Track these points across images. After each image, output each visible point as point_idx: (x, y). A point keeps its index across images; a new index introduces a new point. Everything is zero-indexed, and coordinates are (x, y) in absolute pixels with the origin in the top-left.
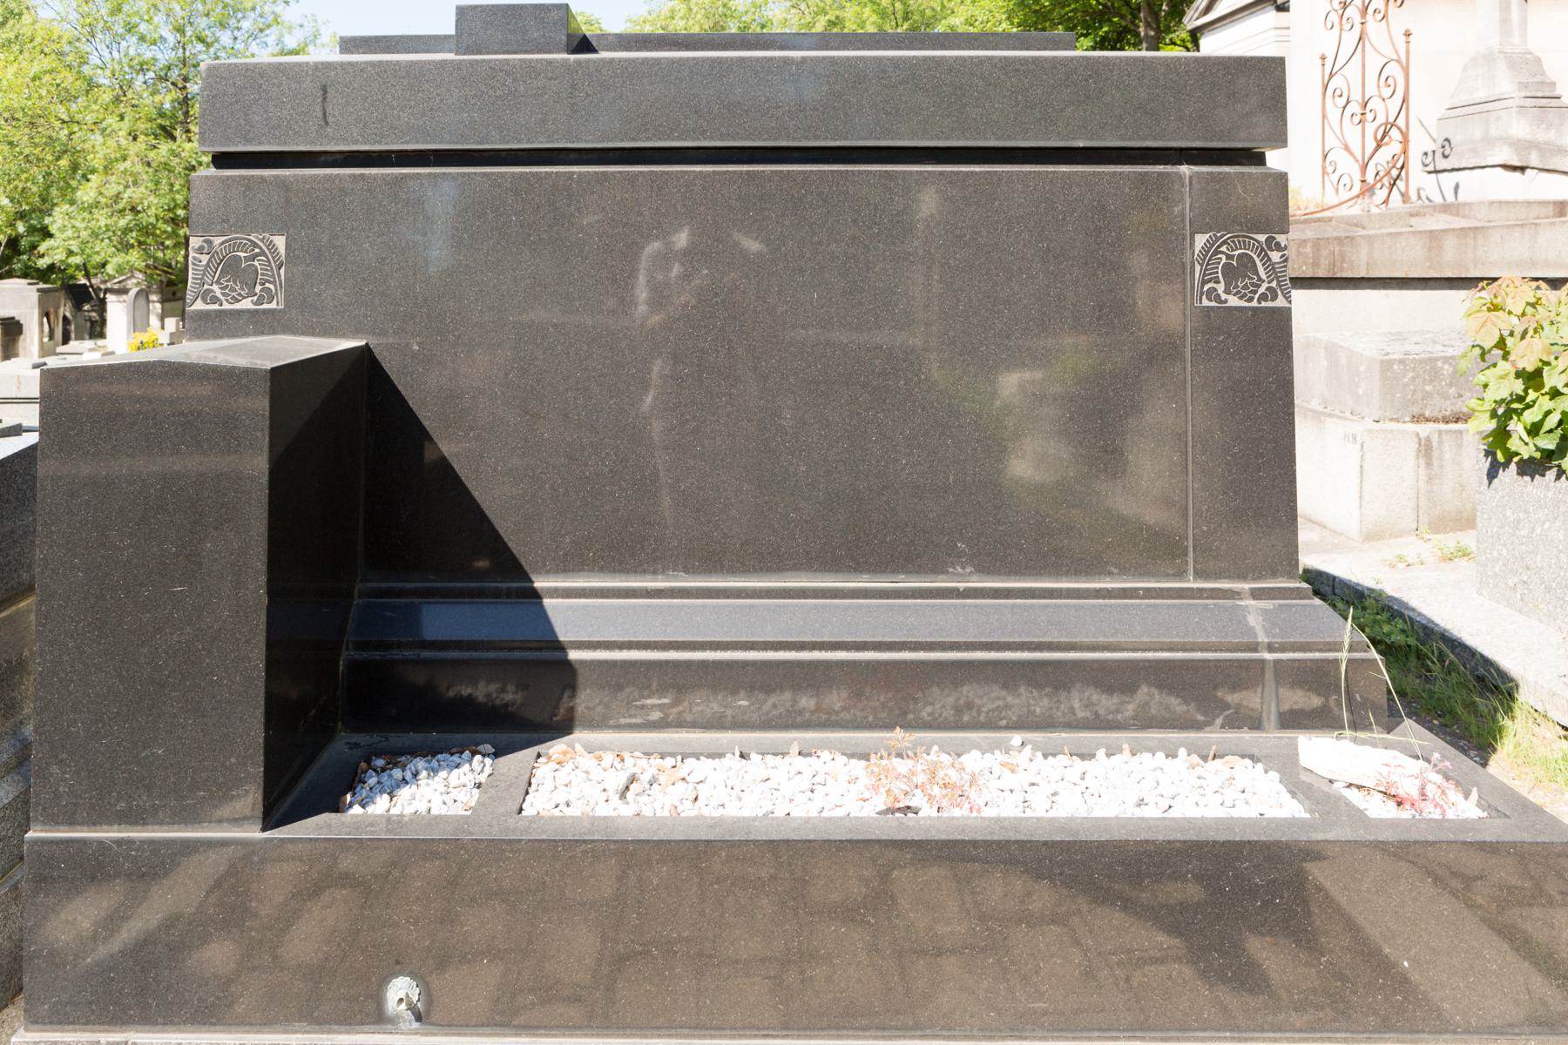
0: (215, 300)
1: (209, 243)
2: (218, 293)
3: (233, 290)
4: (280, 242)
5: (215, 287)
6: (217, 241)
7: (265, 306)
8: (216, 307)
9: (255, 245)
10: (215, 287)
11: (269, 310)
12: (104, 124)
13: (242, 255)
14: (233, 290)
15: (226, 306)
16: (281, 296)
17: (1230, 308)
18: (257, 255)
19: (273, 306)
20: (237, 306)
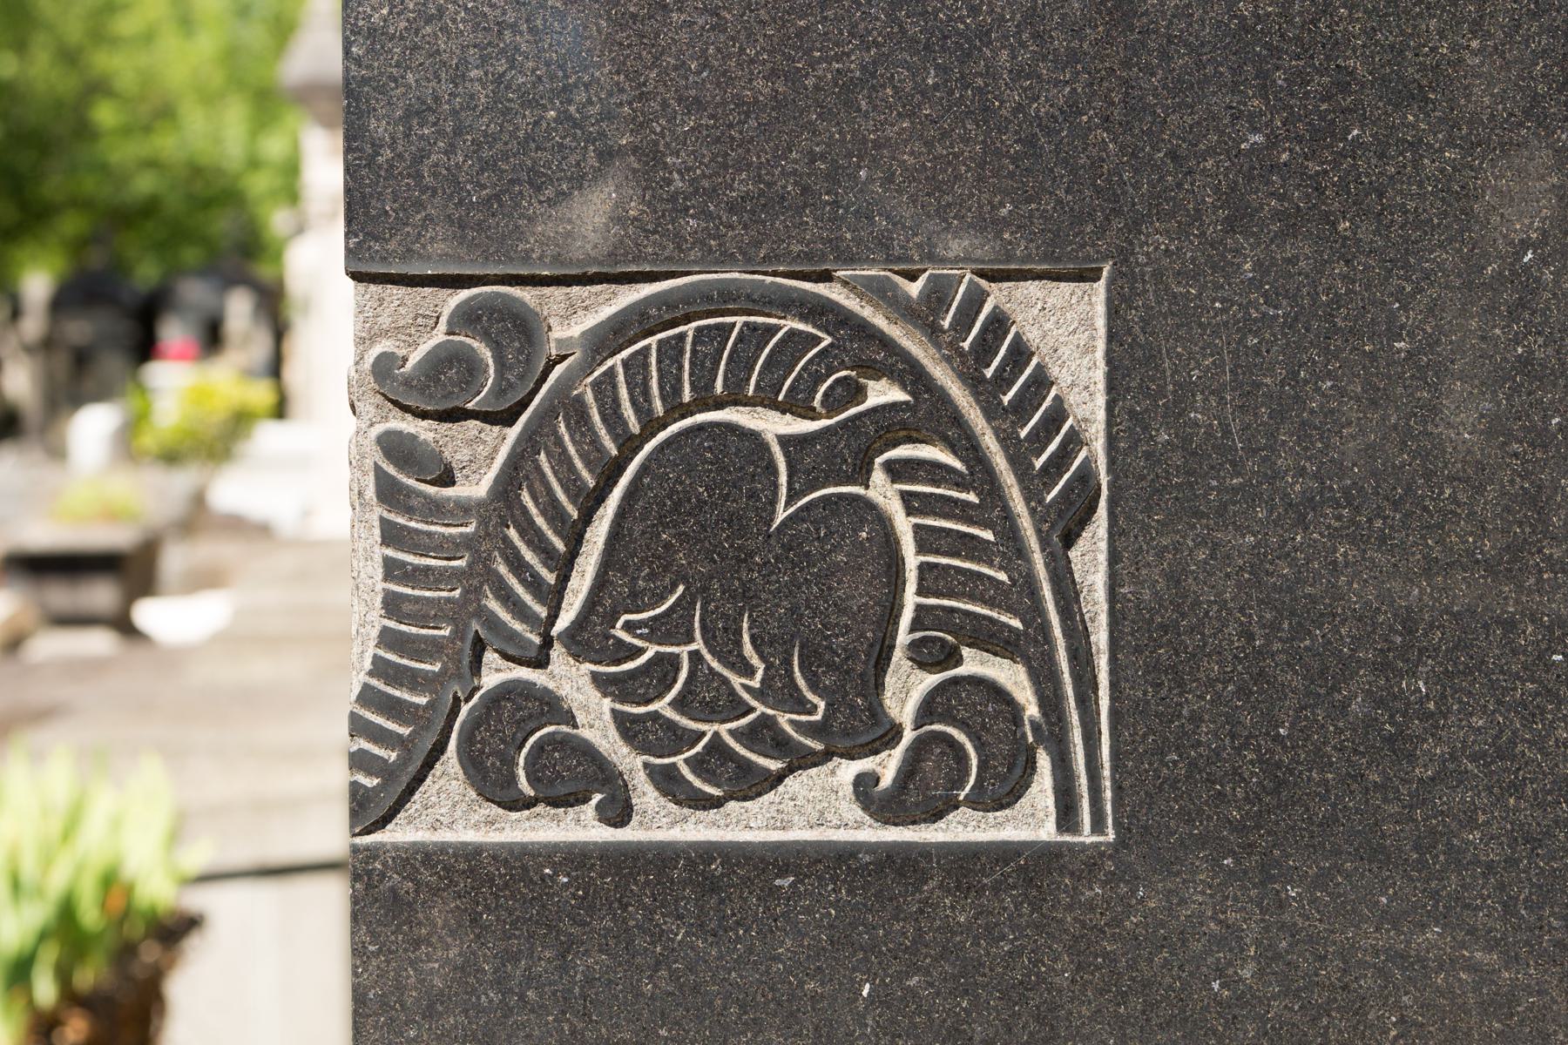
0: (574, 775)
1: (520, 330)
2: (596, 720)
3: (709, 698)
4: (1066, 330)
5: (568, 678)
6: (572, 317)
7: (962, 828)
8: (581, 827)
9: (869, 352)
10: (568, 678)
11: (1005, 853)
12: (1048, 305)
13: (773, 425)
14: (709, 698)
15: (659, 823)
16: (1095, 747)
17: (1045, 714)
18: (890, 426)
19: (1031, 820)
20: (745, 824)
